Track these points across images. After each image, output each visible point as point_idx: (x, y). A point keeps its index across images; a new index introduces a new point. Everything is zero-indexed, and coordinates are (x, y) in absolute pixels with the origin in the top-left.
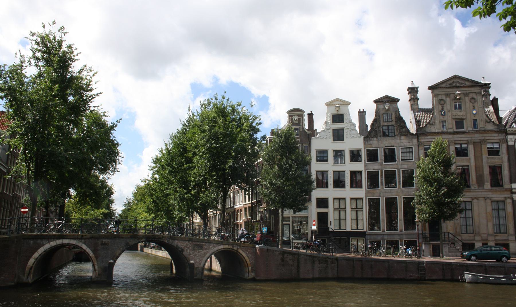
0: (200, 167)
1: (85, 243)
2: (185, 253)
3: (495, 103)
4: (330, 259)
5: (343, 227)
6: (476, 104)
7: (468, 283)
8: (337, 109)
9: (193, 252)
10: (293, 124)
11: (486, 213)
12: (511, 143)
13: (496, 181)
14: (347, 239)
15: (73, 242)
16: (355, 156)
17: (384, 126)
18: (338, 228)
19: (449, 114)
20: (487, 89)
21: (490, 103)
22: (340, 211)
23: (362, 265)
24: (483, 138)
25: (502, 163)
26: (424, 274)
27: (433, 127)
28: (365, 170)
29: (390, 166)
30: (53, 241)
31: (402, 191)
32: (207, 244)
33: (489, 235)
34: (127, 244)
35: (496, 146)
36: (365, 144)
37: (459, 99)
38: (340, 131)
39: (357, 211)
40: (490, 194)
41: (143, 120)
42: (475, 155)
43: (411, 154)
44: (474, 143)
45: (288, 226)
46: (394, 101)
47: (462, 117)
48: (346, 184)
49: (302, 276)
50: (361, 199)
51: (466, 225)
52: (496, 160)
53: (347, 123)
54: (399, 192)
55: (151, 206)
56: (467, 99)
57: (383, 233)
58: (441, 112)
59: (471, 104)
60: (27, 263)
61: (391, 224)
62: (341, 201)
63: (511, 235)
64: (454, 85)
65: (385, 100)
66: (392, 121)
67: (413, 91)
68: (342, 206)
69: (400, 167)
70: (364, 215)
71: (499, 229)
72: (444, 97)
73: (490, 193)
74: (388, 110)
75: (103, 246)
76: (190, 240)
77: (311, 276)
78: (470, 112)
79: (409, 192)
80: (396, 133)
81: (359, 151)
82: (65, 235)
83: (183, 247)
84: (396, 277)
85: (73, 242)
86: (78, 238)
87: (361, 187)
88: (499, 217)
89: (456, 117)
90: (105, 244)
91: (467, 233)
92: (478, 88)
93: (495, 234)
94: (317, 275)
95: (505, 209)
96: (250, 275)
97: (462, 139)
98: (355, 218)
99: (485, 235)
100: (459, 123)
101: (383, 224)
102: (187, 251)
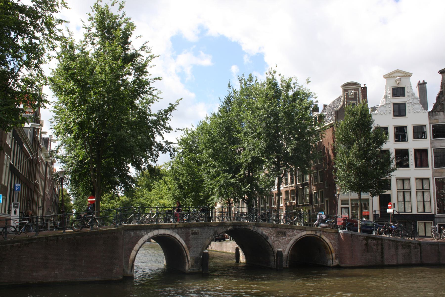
0: (248, 148)
1: (178, 233)
2: (269, 240)
4: (413, 244)
9: (277, 239)
10: (348, 99)
14: (413, 223)
15: (168, 232)
16: (419, 132)
18: (403, 211)
28: (432, 147)
30: (151, 231)
32: (291, 230)
34: (215, 233)
36: (430, 119)
38: (401, 106)
41: (184, 100)
48: (410, 163)
49: (386, 263)
53: (408, 96)
55: (177, 193)
60: (130, 256)
68: (407, 187)
75: (193, 236)
77: (395, 263)
82: (161, 225)
83: (267, 234)
85: (168, 232)
86: (172, 228)
87: (427, 166)
94: (401, 262)
96: (334, 262)
98: (422, 200)
102: (271, 238)
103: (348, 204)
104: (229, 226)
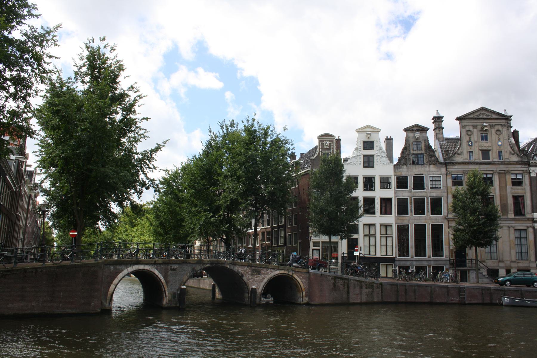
1: (157, 269)
2: (244, 278)
3: (515, 134)
5: (372, 253)
6: (501, 136)
7: (506, 306)
8: (369, 136)
11: (510, 241)
12: (533, 175)
13: (519, 211)
14: (376, 265)
16: (385, 183)
17: (414, 154)
19: (476, 145)
20: (509, 122)
21: (511, 135)
22: (369, 237)
23: (406, 289)
24: (508, 169)
25: (525, 193)
26: (464, 298)
27: (460, 157)
29: (419, 194)
31: (431, 219)
32: (265, 269)
33: (511, 262)
35: (519, 177)
36: (395, 171)
37: (486, 130)
38: (371, 158)
39: (386, 237)
40: (513, 223)
41: (170, 140)
42: (500, 186)
43: (439, 183)
44: (499, 173)
45: (318, 251)
46: (424, 130)
47: (488, 148)
48: (376, 211)
49: (351, 301)
50: (391, 226)
51: (491, 252)
52: (520, 191)
53: (377, 150)
54: (428, 219)
56: (493, 131)
57: (412, 259)
58: (469, 142)
59: (497, 136)
61: (420, 250)
62: (388, 228)
63: (533, 262)
64: (481, 116)
65: (415, 128)
66: (421, 150)
67: (438, 120)
68: (372, 232)
69: (429, 195)
70: (394, 241)
71: (522, 255)
72: (471, 128)
73: (514, 222)
74: (417, 139)
76: (249, 266)
77: (359, 301)
78: (497, 143)
79: (437, 219)
80: (425, 161)
81: (388, 178)
82: (141, 261)
83: (243, 272)
84: (438, 301)
87: (391, 214)
88: (521, 245)
89: (483, 148)
90: (174, 270)
91: (491, 259)
92: (504, 121)
93: (517, 261)
94: (364, 300)
95: (526, 237)
97: (488, 169)
98: (385, 244)
99: (509, 262)
100: (485, 154)
101: (412, 250)
103: (319, 246)
104: (207, 264)
